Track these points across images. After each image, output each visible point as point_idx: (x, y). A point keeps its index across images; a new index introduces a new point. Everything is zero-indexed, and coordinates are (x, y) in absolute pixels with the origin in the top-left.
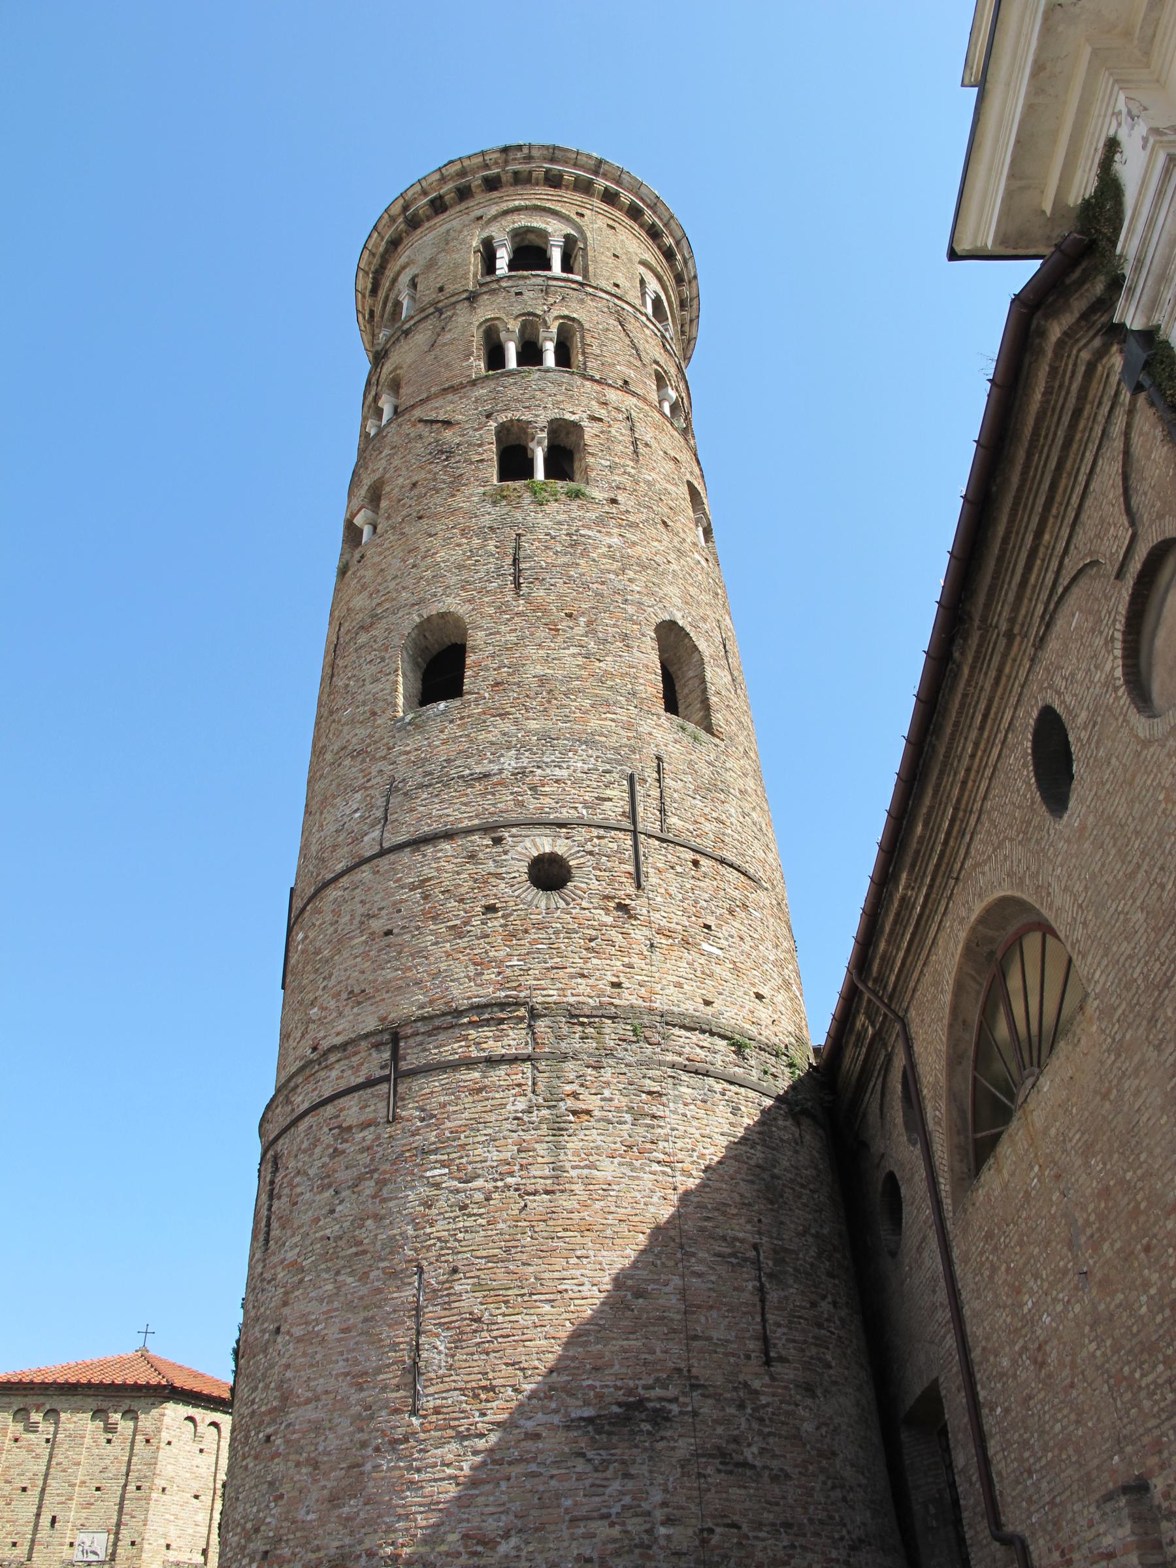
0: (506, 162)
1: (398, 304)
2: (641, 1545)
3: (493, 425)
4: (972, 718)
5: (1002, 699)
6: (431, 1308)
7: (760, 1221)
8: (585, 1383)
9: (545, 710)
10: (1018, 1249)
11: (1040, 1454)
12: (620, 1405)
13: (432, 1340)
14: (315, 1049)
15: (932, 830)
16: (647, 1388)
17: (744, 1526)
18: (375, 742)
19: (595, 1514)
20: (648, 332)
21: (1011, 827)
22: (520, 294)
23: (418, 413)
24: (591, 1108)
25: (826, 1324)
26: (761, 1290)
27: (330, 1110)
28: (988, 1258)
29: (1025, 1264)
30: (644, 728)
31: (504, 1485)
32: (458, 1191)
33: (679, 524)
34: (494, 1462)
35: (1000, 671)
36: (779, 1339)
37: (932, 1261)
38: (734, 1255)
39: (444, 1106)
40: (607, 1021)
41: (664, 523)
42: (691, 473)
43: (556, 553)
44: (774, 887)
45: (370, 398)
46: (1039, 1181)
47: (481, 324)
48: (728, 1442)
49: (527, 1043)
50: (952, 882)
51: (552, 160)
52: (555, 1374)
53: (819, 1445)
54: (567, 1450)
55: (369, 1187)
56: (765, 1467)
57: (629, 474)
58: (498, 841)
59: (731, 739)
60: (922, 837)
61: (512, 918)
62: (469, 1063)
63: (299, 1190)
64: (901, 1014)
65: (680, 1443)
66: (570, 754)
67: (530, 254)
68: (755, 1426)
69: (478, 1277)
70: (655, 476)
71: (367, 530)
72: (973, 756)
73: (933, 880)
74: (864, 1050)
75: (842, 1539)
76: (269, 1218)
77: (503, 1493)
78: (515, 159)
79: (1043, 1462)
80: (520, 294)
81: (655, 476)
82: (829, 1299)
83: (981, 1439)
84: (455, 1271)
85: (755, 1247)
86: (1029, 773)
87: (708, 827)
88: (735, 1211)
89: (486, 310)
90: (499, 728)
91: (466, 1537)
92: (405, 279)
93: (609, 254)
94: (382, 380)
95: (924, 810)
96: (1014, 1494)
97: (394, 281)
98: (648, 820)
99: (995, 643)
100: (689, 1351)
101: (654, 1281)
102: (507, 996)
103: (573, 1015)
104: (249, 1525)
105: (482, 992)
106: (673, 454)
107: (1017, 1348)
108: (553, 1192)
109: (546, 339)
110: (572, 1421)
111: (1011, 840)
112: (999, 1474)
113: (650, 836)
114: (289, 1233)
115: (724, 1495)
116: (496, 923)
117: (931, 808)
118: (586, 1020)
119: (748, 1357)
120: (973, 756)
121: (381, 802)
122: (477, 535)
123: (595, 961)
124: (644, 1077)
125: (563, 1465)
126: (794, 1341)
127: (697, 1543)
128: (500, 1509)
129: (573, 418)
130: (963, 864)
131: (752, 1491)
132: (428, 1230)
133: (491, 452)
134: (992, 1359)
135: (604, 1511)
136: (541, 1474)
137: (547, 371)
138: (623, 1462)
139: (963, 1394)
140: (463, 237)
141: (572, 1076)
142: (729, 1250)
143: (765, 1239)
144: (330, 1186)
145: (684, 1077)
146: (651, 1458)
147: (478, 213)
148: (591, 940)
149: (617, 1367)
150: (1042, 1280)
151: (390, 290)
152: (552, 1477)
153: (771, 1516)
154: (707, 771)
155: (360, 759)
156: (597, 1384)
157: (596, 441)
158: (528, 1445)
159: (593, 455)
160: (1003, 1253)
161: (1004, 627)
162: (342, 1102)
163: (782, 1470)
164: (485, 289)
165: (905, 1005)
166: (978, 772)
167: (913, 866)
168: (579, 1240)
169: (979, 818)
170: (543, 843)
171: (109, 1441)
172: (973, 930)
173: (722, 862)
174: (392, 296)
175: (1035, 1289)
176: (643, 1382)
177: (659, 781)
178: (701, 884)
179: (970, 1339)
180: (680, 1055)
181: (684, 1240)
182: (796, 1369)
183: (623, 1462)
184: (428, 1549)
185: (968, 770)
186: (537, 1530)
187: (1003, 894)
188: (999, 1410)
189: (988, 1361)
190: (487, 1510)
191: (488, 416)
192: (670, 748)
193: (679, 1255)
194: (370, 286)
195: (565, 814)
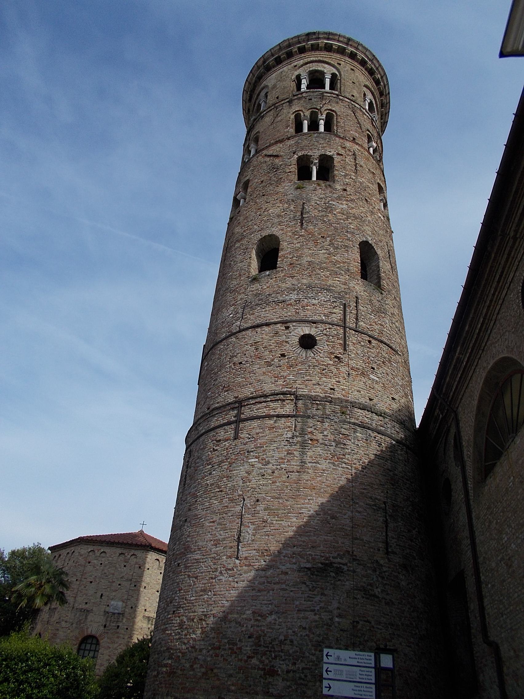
0: (308, 41)
1: (259, 105)
2: (327, 625)
3: (296, 156)
4: (495, 277)
5: (509, 268)
6: (247, 516)
7: (387, 492)
8: (308, 553)
9: (310, 276)
10: (502, 514)
11: (507, 607)
12: (322, 564)
13: (246, 528)
14: (208, 409)
15: (473, 328)
16: (333, 558)
17: (373, 622)
18: (240, 287)
19: (308, 609)
20: (365, 117)
21: (509, 326)
22: (311, 99)
23: (265, 152)
24: (318, 438)
25: (414, 540)
26: (386, 522)
27: (212, 433)
28: (488, 517)
29: (505, 521)
30: (351, 285)
31: (271, 592)
32: (261, 469)
33: (372, 201)
34: (268, 582)
35: (509, 255)
36: (393, 544)
37: (463, 518)
38: (375, 505)
39: (258, 434)
40: (327, 403)
41: (366, 200)
42: (380, 179)
43: (319, 211)
44: (403, 355)
45: (246, 146)
46: (513, 484)
47: (293, 113)
48: (368, 585)
49: (294, 410)
50: (481, 352)
51: (328, 39)
52: (295, 548)
53: (408, 592)
54: (298, 580)
55: (225, 466)
56: (383, 598)
57: (352, 179)
58: (287, 328)
59: (389, 292)
60: (468, 331)
61: (291, 359)
62: (269, 417)
63: (198, 465)
64: (455, 409)
65: (347, 583)
66: (320, 294)
67: (316, 80)
68: (380, 579)
69: (267, 504)
70: (364, 180)
71: (242, 201)
72: (494, 295)
73: (472, 351)
74: (438, 425)
75: (416, 634)
76: (186, 476)
77: (270, 596)
78: (312, 39)
79: (509, 610)
80: (311, 99)
81: (364, 180)
82: (417, 530)
83: (481, 598)
84: (258, 501)
85: (385, 503)
86: (519, 301)
87: (376, 327)
88: (377, 487)
89: (296, 107)
90: (289, 283)
91: (254, 613)
92: (263, 94)
93: (351, 82)
94: (252, 138)
95: (470, 319)
96: (494, 623)
97: (258, 95)
98: (351, 323)
99: (508, 242)
100: (353, 544)
101: (340, 513)
102: (287, 391)
103: (313, 399)
104: (168, 600)
105: (277, 389)
106: (372, 170)
107: (499, 558)
108: (300, 472)
109: (321, 119)
110: (301, 568)
111: (509, 331)
112: (488, 614)
113: (350, 329)
114: (193, 481)
115: (365, 608)
116: (284, 361)
117: (473, 318)
118: (318, 402)
119: (379, 550)
120: (494, 295)
121: (240, 311)
122: (287, 203)
123: (324, 379)
124: (342, 428)
125: (297, 586)
126: (399, 546)
127: (351, 627)
128: (269, 602)
129: (330, 154)
130: (486, 343)
131: (377, 608)
132: (248, 484)
133: (294, 168)
134: (487, 562)
135: (312, 608)
136: (287, 589)
137: (321, 133)
138: (322, 588)
139: (474, 577)
140: (288, 72)
141: (311, 425)
142: (373, 503)
143: (389, 500)
144: (210, 464)
145: (359, 429)
146: (334, 588)
147: (295, 64)
148: (323, 370)
149: (322, 547)
150: (512, 528)
151: (257, 99)
152: (291, 591)
153: (385, 620)
154: (377, 304)
155: (233, 294)
156: (313, 554)
157: (339, 164)
158: (283, 577)
159: (337, 170)
160: (495, 515)
161: (512, 234)
162: (218, 430)
163: (390, 600)
164: (296, 97)
165: (457, 405)
166: (496, 302)
167: (463, 344)
168: (310, 492)
169: (495, 322)
170: (306, 330)
171: (125, 566)
172: (489, 372)
173: (382, 342)
174: (257, 102)
175: (509, 532)
176: (332, 555)
177: (356, 307)
178: (372, 350)
179: (478, 553)
180: (358, 419)
181: (354, 497)
182: (399, 557)
183: (322, 588)
184: (238, 616)
185: (491, 301)
186: (283, 613)
187: (504, 356)
188: (490, 586)
189: (486, 563)
190: (264, 602)
191: (294, 153)
192: (362, 294)
193: (351, 503)
194: (248, 98)
195: (316, 318)
